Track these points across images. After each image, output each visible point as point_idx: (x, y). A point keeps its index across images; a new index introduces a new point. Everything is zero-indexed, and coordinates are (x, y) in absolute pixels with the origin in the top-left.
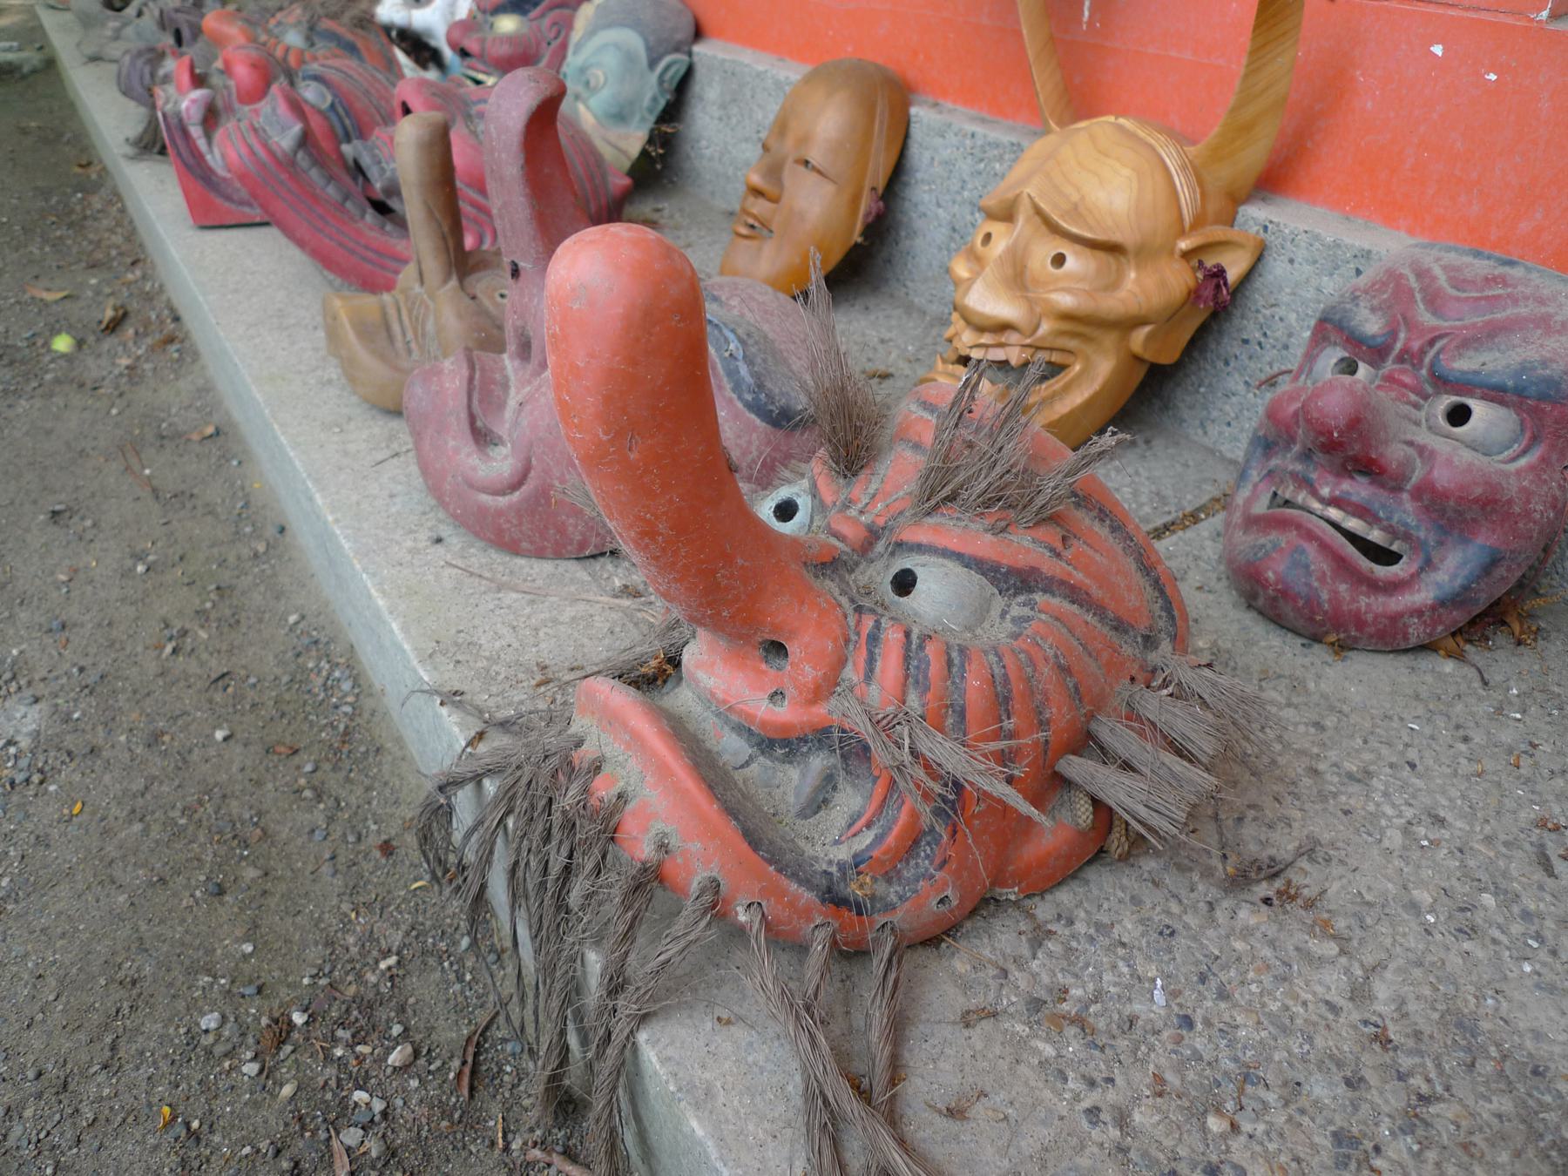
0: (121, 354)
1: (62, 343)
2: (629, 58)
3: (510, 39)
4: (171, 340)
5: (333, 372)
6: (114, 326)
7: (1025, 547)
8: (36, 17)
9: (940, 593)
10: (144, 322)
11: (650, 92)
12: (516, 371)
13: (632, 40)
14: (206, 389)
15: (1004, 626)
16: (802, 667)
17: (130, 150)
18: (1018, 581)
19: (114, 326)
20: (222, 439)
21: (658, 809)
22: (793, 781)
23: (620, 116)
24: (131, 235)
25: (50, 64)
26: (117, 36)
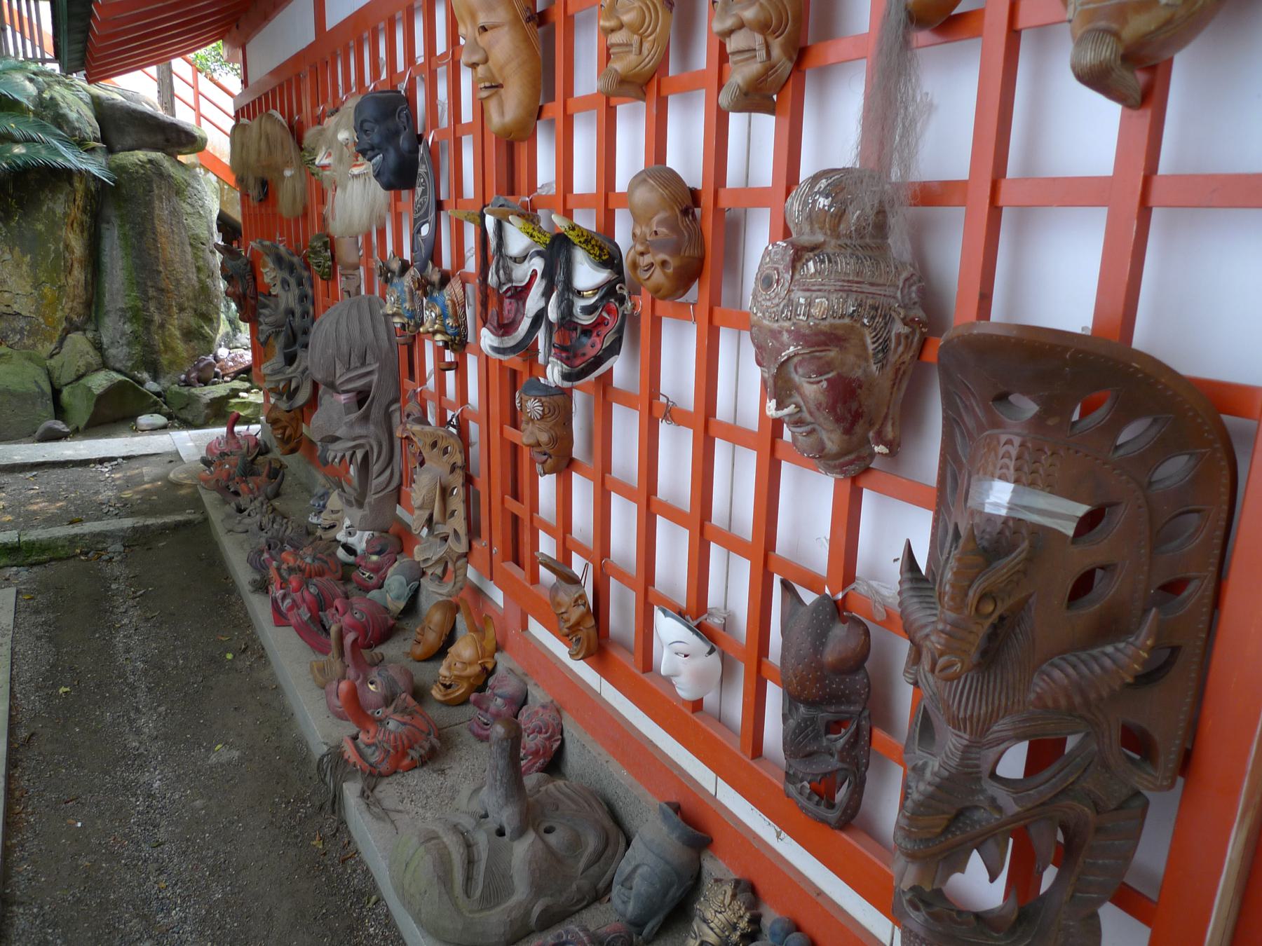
0: (246, 662)
1: (229, 656)
2: (401, 584)
3: (375, 563)
4: (261, 657)
5: (311, 677)
6: (244, 651)
7: (407, 718)
8: (197, 491)
9: (392, 725)
10: (255, 651)
11: (407, 592)
12: (588, 382)
13: (403, 579)
14: (273, 674)
15: (401, 729)
16: (372, 733)
17: (250, 588)
18: (405, 724)
19: (244, 651)
20: (277, 690)
21: (349, 752)
22: (369, 751)
23: (398, 598)
24: (246, 614)
25: (206, 520)
26: (240, 522)
